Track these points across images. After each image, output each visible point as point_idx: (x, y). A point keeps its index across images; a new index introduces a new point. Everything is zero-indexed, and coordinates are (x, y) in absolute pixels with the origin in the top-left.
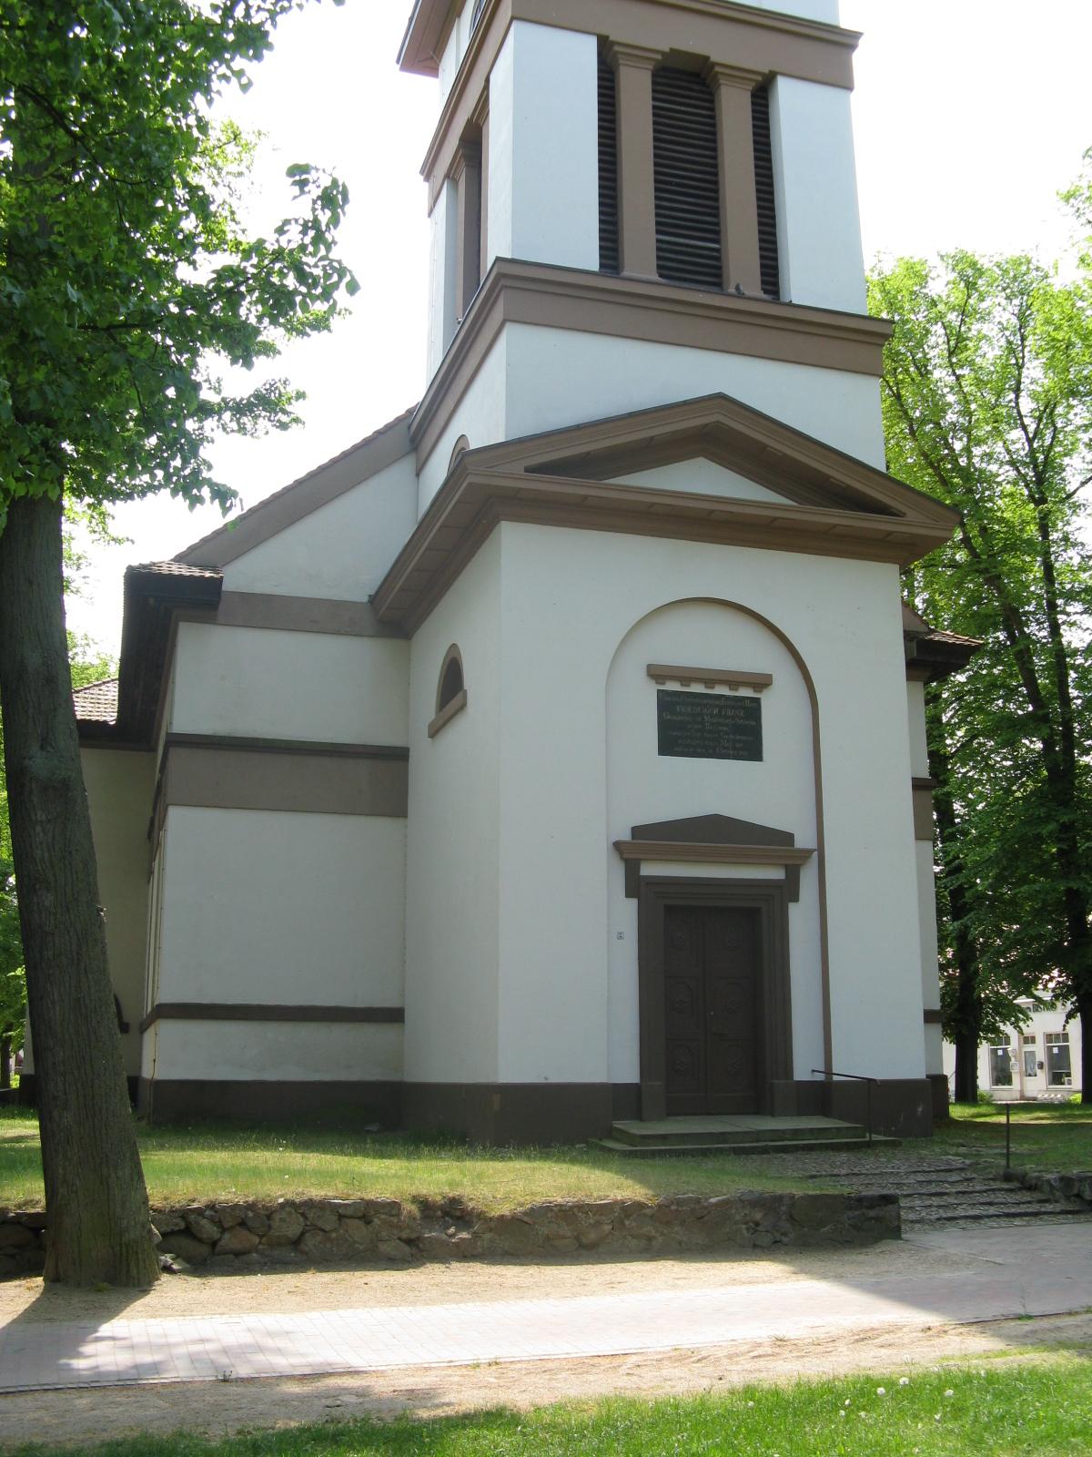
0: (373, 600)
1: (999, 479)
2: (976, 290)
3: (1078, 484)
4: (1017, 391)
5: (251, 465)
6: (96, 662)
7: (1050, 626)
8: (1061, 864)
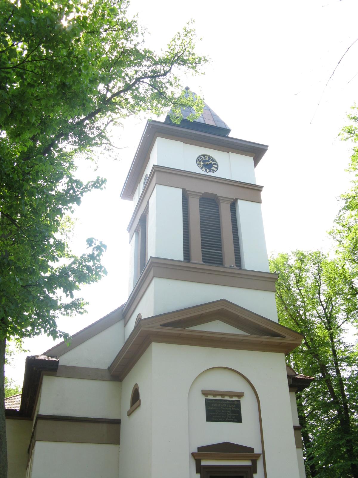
0: (109, 368)
1: (315, 322)
2: (304, 262)
3: (341, 323)
4: (319, 293)
5: (69, 324)
6: (14, 388)
7: (336, 371)
8: (348, 455)
